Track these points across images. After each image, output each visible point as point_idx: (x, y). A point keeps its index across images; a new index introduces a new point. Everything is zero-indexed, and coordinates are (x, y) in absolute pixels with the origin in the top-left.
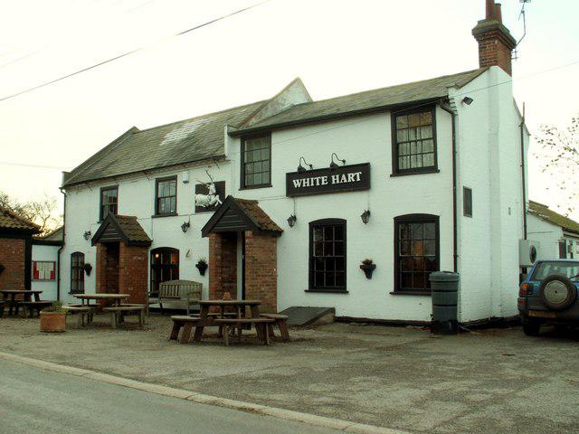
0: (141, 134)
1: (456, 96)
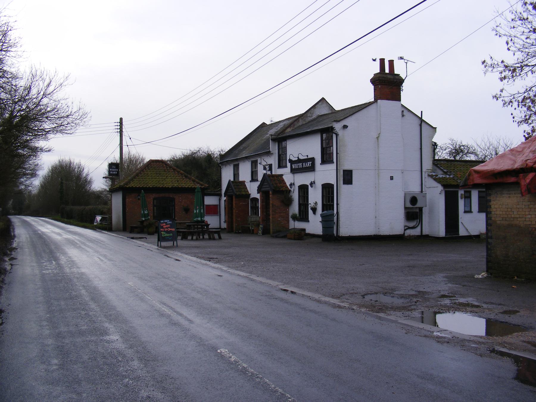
1: (338, 127)
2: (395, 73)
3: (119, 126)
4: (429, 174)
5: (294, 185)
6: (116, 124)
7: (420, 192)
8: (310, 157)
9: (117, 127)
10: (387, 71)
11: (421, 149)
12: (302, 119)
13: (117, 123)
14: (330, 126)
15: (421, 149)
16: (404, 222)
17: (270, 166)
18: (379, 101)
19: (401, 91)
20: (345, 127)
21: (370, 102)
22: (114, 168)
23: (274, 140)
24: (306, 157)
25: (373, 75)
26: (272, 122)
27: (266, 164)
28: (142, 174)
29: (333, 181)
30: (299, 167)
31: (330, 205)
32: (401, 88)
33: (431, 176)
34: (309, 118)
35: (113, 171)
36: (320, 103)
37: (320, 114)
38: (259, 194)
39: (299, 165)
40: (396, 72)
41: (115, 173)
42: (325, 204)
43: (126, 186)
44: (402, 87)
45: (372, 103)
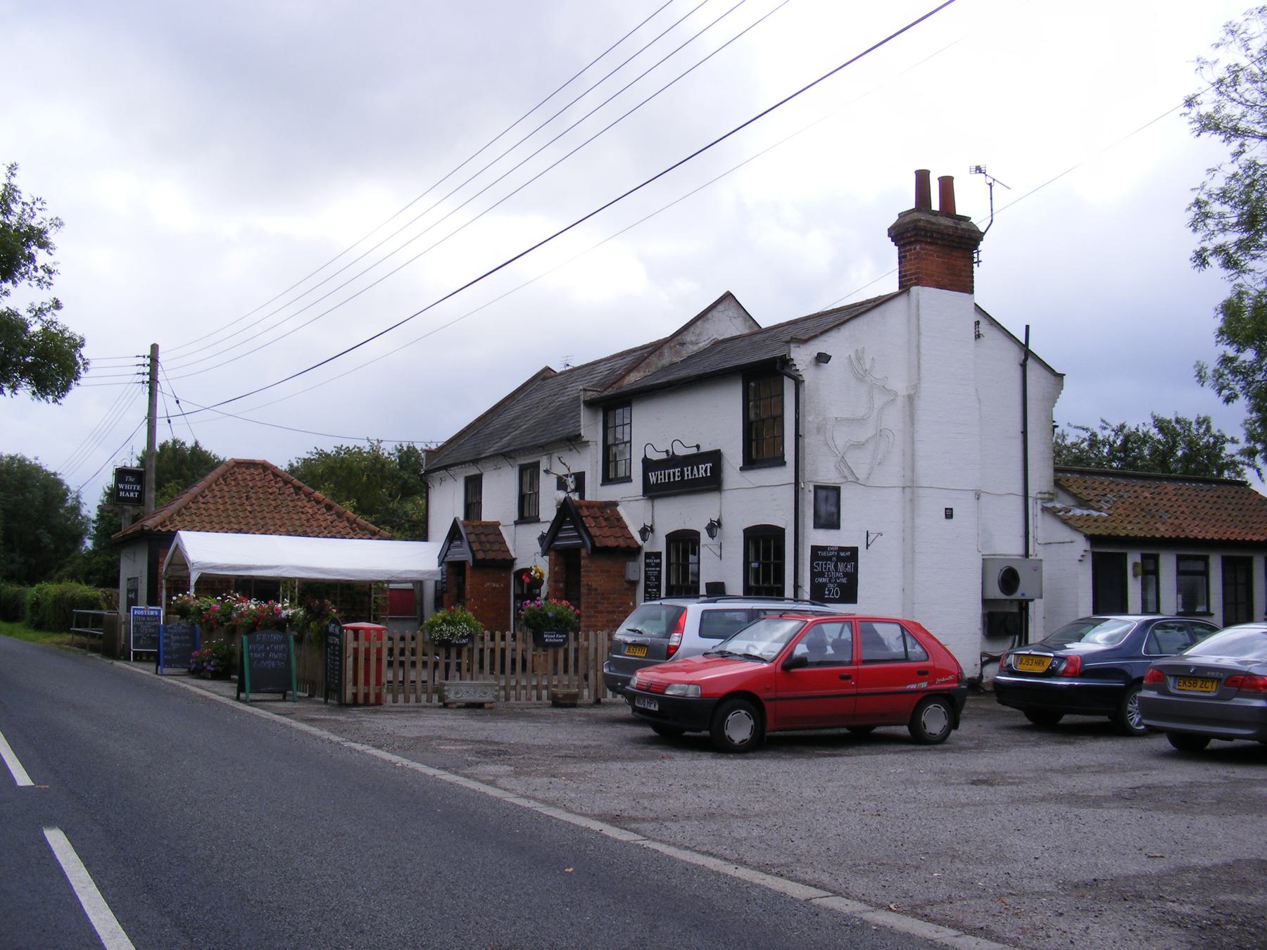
0: (559, 377)
1: (802, 356)
2: (957, 213)
3: (148, 376)
4: (1045, 505)
5: (652, 530)
6: (141, 361)
7: (1022, 556)
8: (705, 448)
9: (141, 378)
10: (935, 205)
11: (1024, 433)
12: (671, 348)
13: (144, 357)
14: (778, 353)
15: (1024, 433)
16: (981, 643)
17: (580, 478)
18: (914, 289)
19: (975, 265)
20: (822, 358)
21: (880, 298)
22: (129, 483)
23: (591, 404)
24: (694, 451)
25: (898, 218)
26: (568, 368)
27: (567, 472)
28: (206, 498)
29: (782, 518)
30: (672, 480)
31: (778, 588)
32: (975, 255)
33: (1053, 512)
34: (691, 347)
35: (125, 491)
36: (720, 307)
37: (721, 338)
38: (547, 558)
39: (669, 474)
40: (960, 211)
41: (132, 495)
42: (753, 587)
43: (159, 528)
44: (978, 252)
45: (884, 299)
